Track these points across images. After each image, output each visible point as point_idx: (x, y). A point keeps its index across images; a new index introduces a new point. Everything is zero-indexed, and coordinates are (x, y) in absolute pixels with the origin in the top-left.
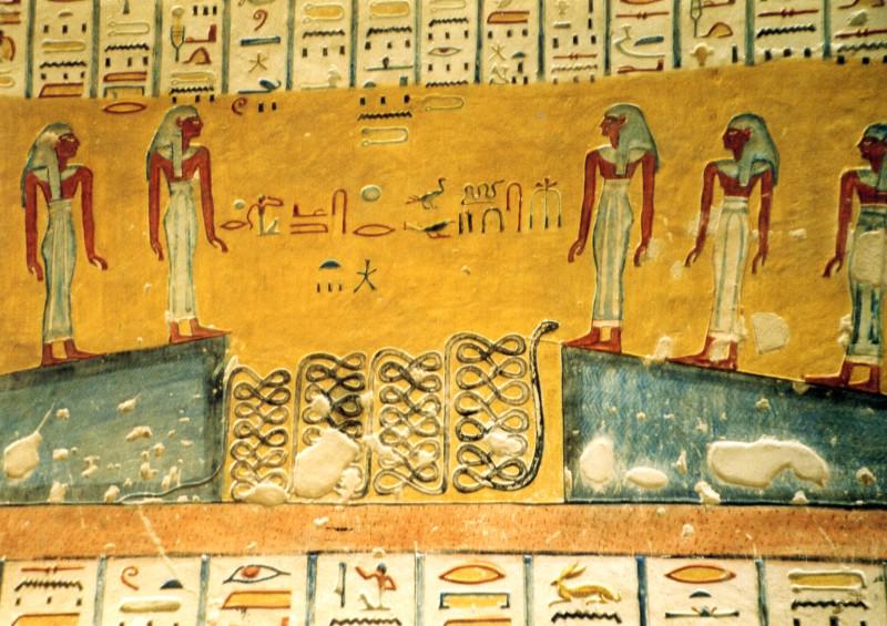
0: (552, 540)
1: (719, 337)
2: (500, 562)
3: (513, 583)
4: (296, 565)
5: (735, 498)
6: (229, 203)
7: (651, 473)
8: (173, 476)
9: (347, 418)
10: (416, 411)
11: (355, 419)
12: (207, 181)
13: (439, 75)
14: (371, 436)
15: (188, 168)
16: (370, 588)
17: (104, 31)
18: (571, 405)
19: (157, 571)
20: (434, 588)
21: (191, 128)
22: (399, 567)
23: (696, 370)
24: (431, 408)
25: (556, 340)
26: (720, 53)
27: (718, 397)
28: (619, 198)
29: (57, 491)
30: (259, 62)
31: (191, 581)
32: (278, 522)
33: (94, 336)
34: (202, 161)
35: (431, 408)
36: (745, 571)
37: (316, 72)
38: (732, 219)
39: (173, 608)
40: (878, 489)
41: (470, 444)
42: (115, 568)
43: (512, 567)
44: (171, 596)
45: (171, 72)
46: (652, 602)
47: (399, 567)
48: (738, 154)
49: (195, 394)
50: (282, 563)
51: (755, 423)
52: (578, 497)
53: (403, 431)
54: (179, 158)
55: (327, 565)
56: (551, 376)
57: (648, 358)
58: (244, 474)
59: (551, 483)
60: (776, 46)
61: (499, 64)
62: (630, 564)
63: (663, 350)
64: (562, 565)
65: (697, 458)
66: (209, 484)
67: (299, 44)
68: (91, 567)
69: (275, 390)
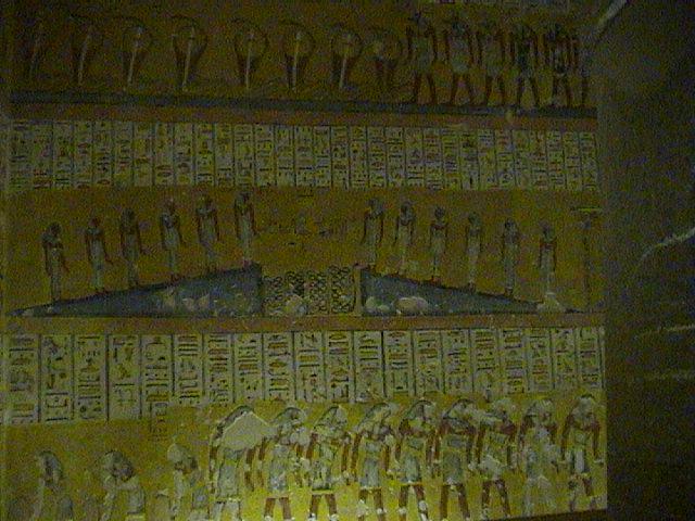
0: (359, 327)
1: (402, 268)
2: (346, 333)
3: (348, 339)
4: (288, 335)
5: (406, 314)
6: (260, 222)
7: (383, 307)
8: (249, 309)
9: (300, 291)
10: (319, 289)
11: (349, 466)
12: (252, 215)
13: (321, 184)
14: (307, 297)
15: (246, 210)
16: (309, 342)
17: (217, 164)
18: (363, 287)
19: (248, 337)
20: (327, 341)
21: (246, 197)
22: (318, 335)
23: (394, 277)
24: (324, 289)
25: (358, 268)
26: (399, 182)
27: (401, 284)
28: (374, 224)
29: (216, 314)
30: (266, 177)
31: (259, 341)
32: (283, 323)
33: (222, 263)
34: (250, 208)
35: (324, 289)
36: (408, 334)
37: (284, 180)
38: (403, 233)
39: (254, 347)
40: (550, 484)
41: (335, 299)
42: (236, 337)
43: (348, 334)
44: (253, 344)
45: (239, 178)
46: (386, 342)
47: (318, 335)
48: (548, 428)
49: (254, 282)
50: (285, 334)
51: (409, 293)
52: (365, 314)
53: (316, 296)
54: (244, 207)
55: (298, 336)
56: (357, 279)
57: (383, 274)
58: (270, 308)
59: (357, 313)
60: (413, 182)
61: (339, 183)
62: (379, 333)
63: (387, 271)
64: (360, 334)
65: (397, 302)
66: (261, 310)
67: (278, 170)
68: (229, 336)
69: (277, 283)
